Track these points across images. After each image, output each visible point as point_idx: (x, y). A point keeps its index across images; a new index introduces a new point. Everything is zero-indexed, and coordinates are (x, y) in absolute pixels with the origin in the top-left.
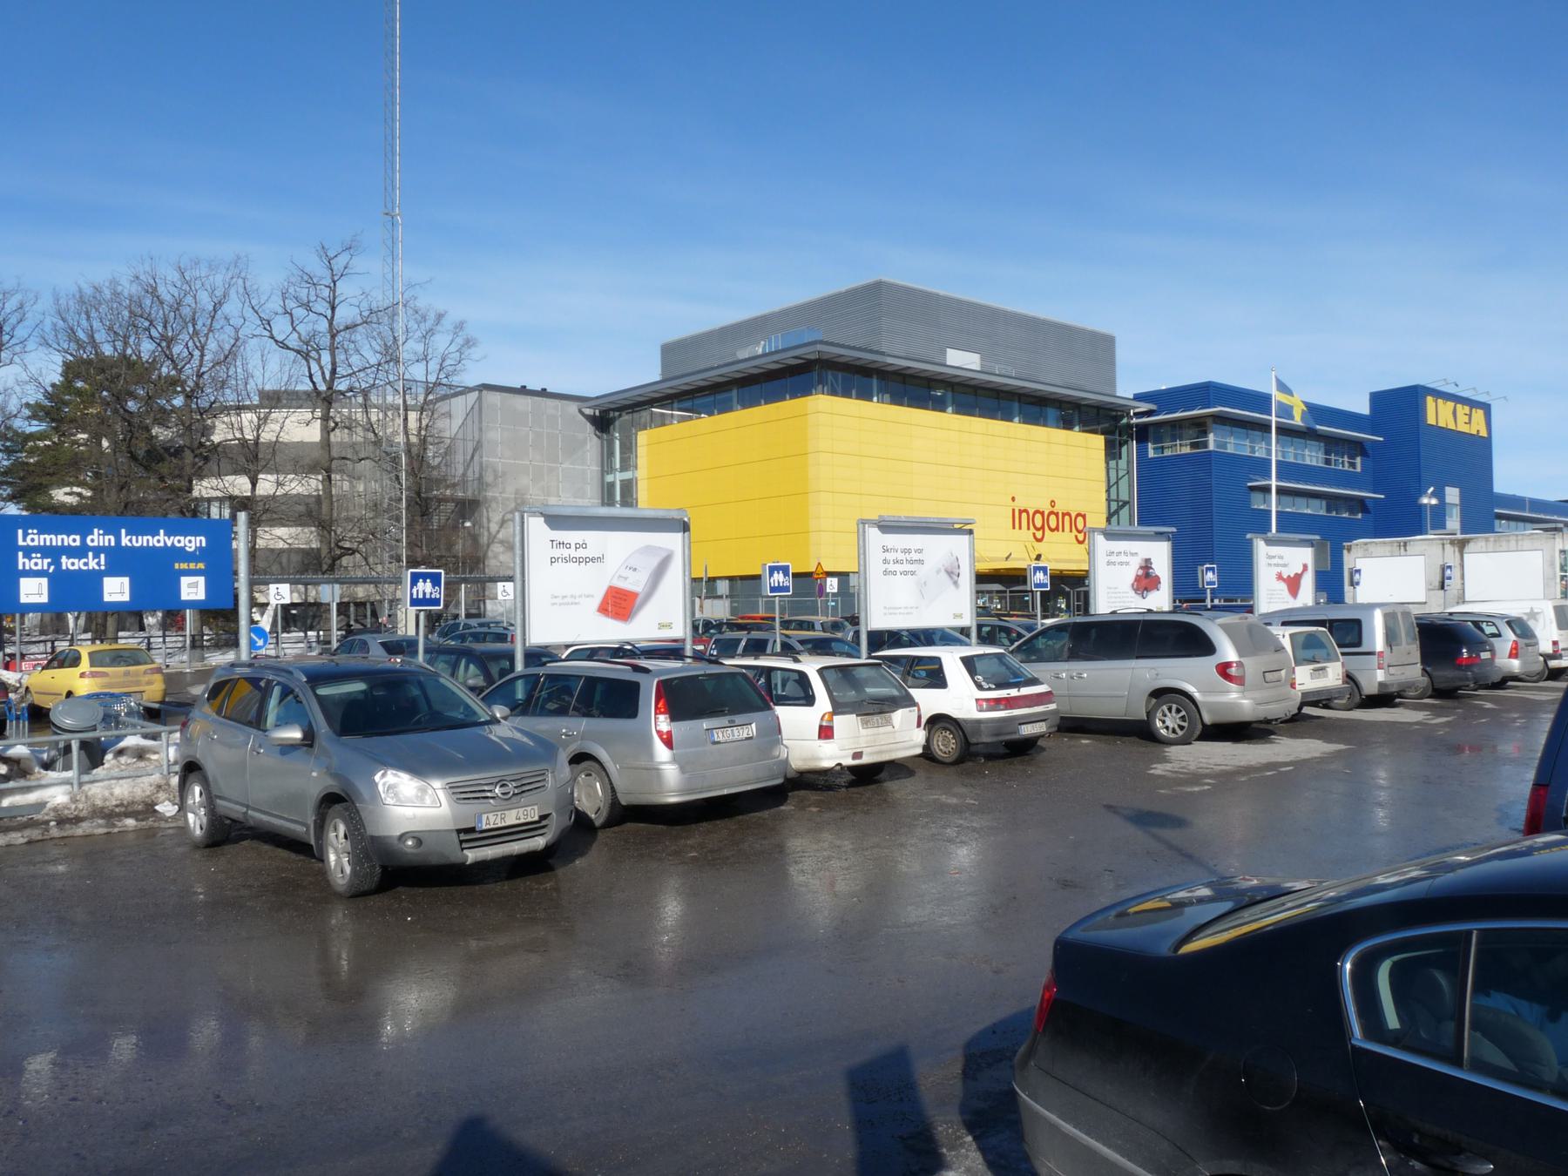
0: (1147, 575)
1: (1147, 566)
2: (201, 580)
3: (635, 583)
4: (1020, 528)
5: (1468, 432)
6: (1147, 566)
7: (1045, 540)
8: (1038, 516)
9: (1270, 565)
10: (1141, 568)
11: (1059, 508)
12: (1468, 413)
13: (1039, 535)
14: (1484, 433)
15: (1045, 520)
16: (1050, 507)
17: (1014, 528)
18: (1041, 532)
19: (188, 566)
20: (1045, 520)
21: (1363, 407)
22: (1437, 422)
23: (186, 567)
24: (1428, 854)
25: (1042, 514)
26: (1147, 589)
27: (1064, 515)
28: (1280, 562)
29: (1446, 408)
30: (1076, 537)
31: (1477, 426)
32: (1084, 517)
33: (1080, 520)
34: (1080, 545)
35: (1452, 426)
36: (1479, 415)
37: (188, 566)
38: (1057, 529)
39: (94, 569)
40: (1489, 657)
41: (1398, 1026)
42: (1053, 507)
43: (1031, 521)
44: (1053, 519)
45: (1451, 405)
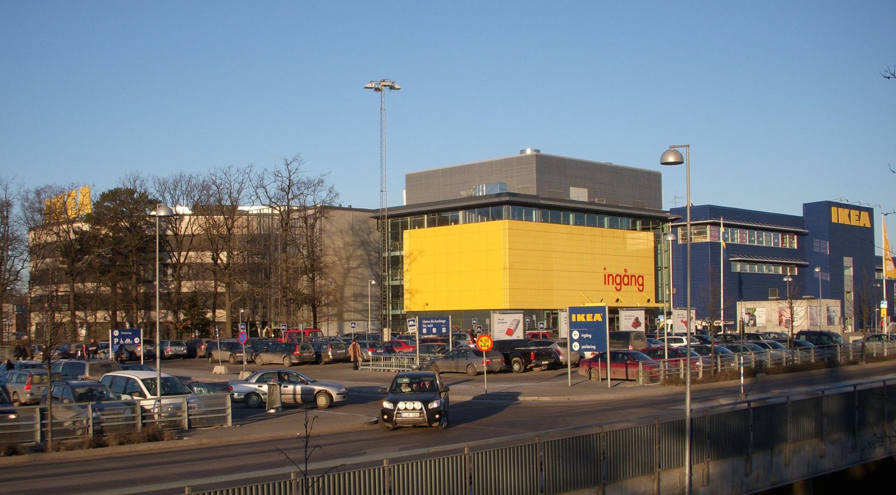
0: (637, 322)
1: (637, 319)
2: (445, 328)
3: (512, 328)
4: (609, 284)
5: (858, 225)
6: (637, 319)
7: (622, 290)
8: (618, 278)
9: (679, 317)
10: (635, 320)
11: (629, 273)
12: (858, 214)
13: (618, 287)
14: (868, 225)
15: (622, 279)
16: (624, 273)
17: (605, 284)
18: (619, 286)
19: (585, 317)
20: (622, 279)
21: (799, 213)
22: (838, 221)
23: (583, 320)
24: (848, 465)
25: (620, 276)
26: (637, 326)
27: (632, 276)
28: (682, 316)
29: (843, 213)
30: (638, 288)
31: (864, 221)
32: (643, 277)
33: (640, 279)
34: (640, 292)
35: (848, 222)
36: (865, 215)
37: (585, 317)
38: (628, 284)
39: (597, 320)
40: (434, 332)
41: (601, 320)
42: (626, 272)
43: (614, 280)
44: (626, 279)
45: (847, 211)
